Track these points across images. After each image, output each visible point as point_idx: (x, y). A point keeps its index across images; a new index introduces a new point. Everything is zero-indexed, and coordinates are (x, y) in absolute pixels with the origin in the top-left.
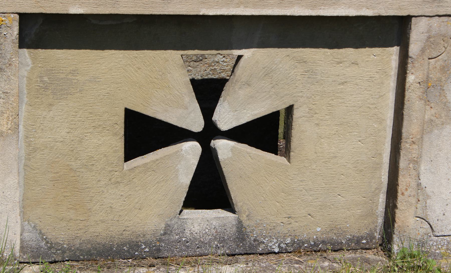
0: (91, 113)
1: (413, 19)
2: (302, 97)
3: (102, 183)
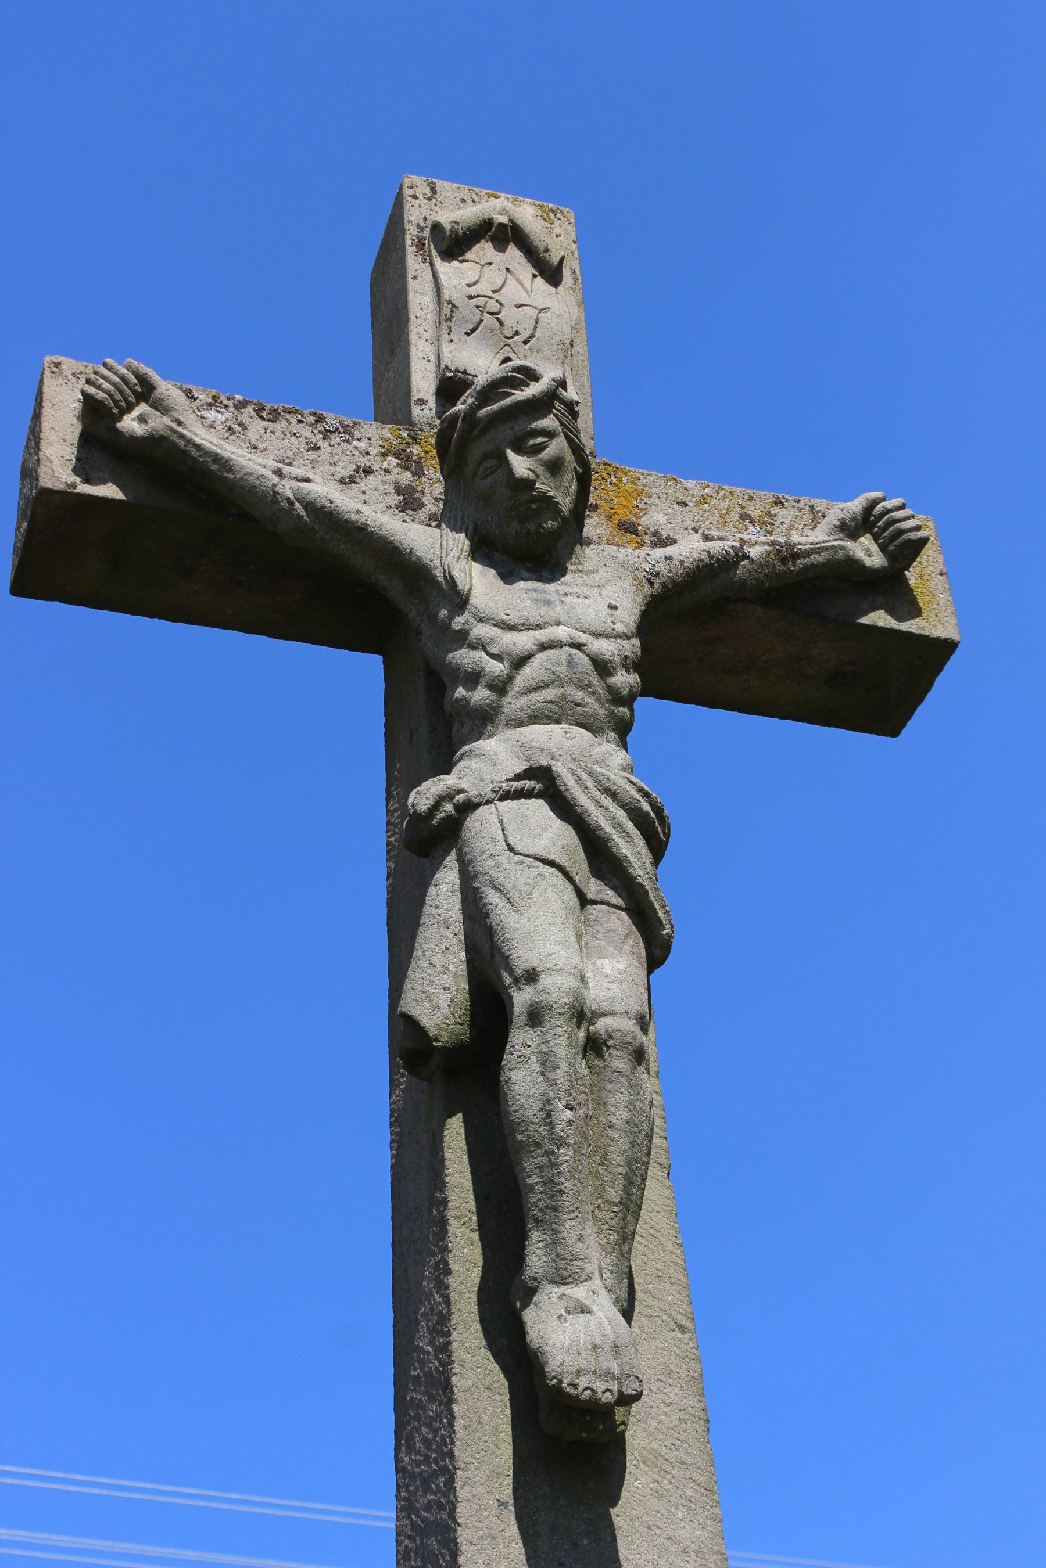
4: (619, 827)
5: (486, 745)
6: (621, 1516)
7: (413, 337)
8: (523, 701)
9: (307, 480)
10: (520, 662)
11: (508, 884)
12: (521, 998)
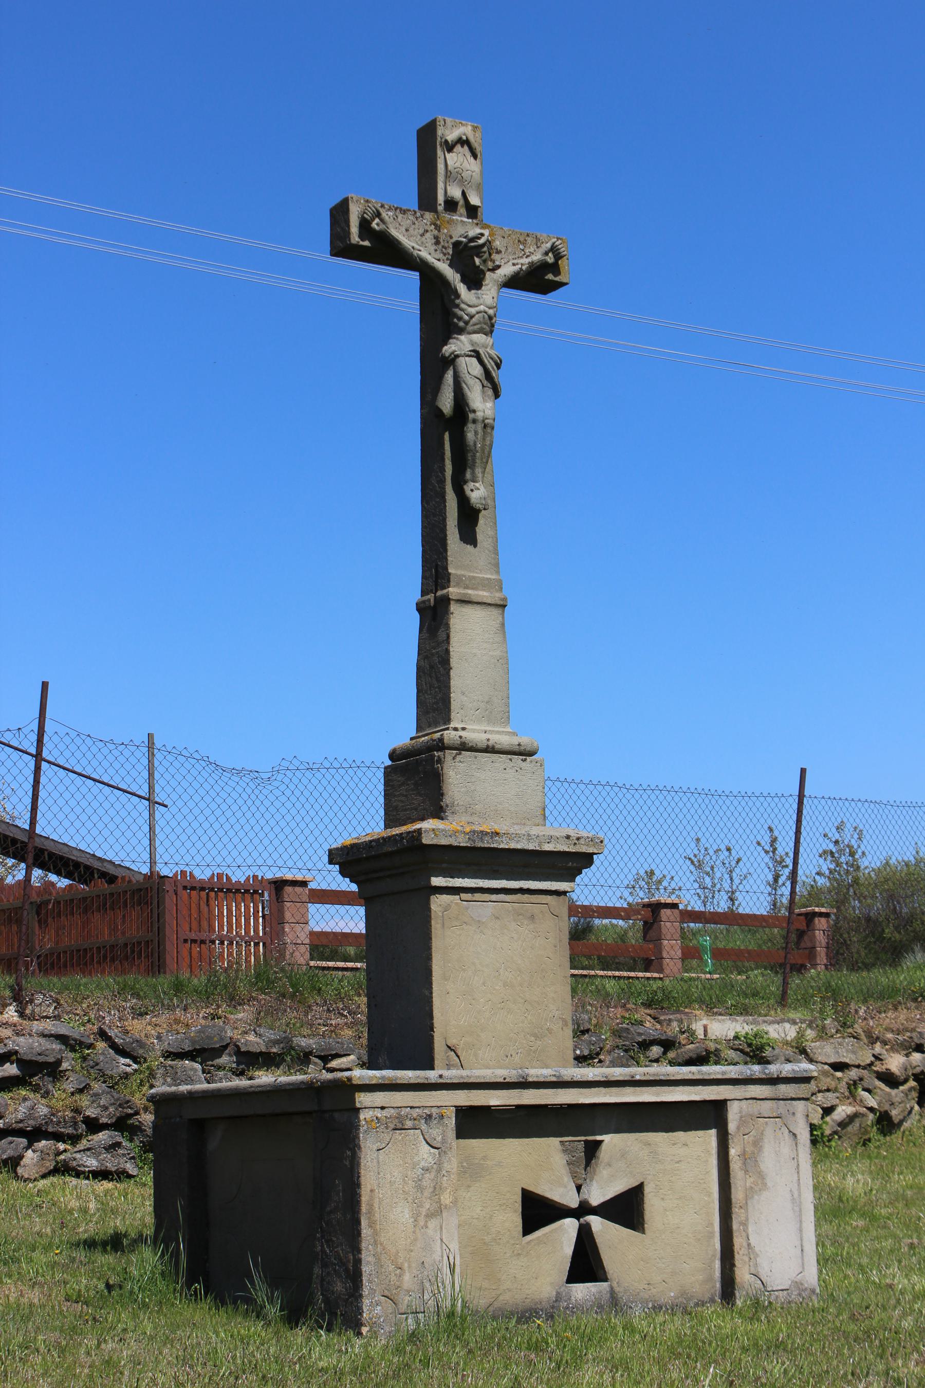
0: (497, 1193)
1: (728, 1102)
2: (649, 1174)
3: (508, 1255)
4: (493, 368)
5: (463, 338)
6: (478, 529)
7: (438, 180)
8: (472, 328)
9: (420, 251)
10: (472, 317)
11: (468, 383)
12: (471, 416)
